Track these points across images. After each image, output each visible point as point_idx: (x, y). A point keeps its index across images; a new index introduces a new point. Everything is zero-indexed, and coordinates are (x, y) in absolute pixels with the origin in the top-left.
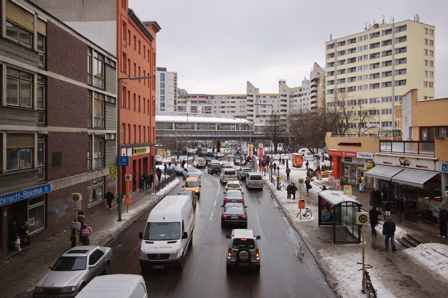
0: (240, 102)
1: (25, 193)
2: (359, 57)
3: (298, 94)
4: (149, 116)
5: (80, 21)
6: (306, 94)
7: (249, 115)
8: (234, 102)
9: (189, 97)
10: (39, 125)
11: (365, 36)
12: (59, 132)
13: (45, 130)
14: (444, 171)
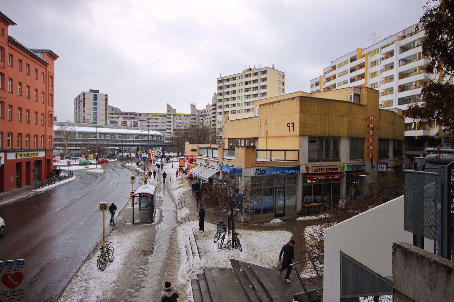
11: (242, 76)
14: (258, 174)
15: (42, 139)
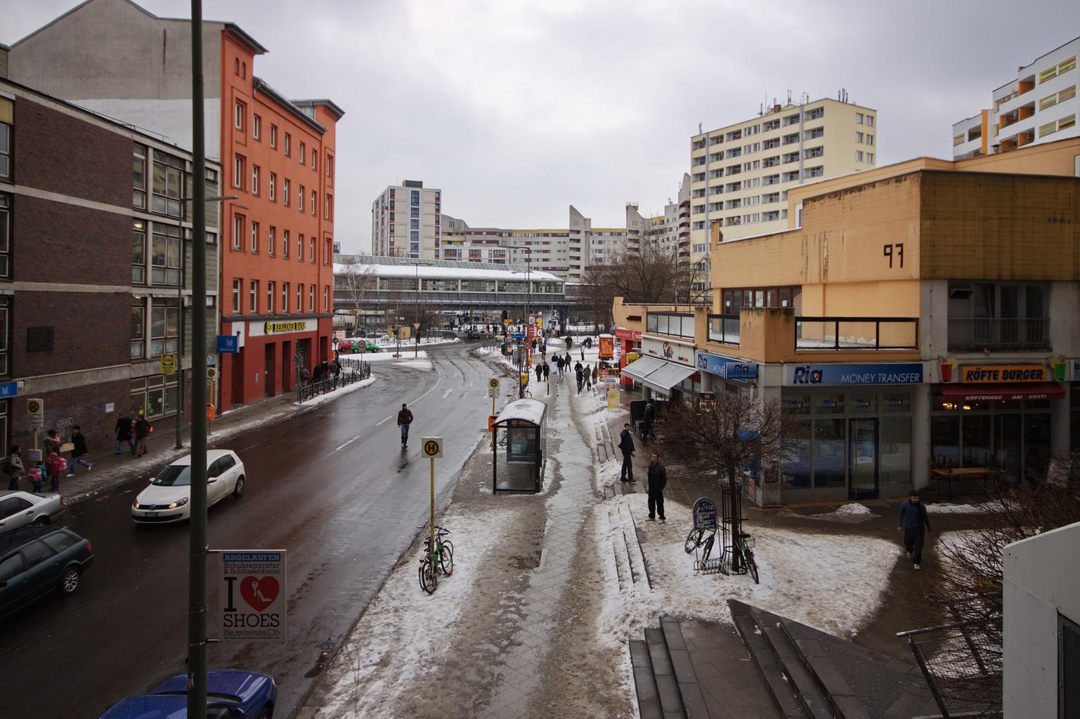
2: (745, 164)
4: (316, 266)
5: (159, 98)
7: (572, 266)
8: (547, 243)
9: (469, 233)
11: (756, 127)
14: (801, 382)
15: (284, 290)
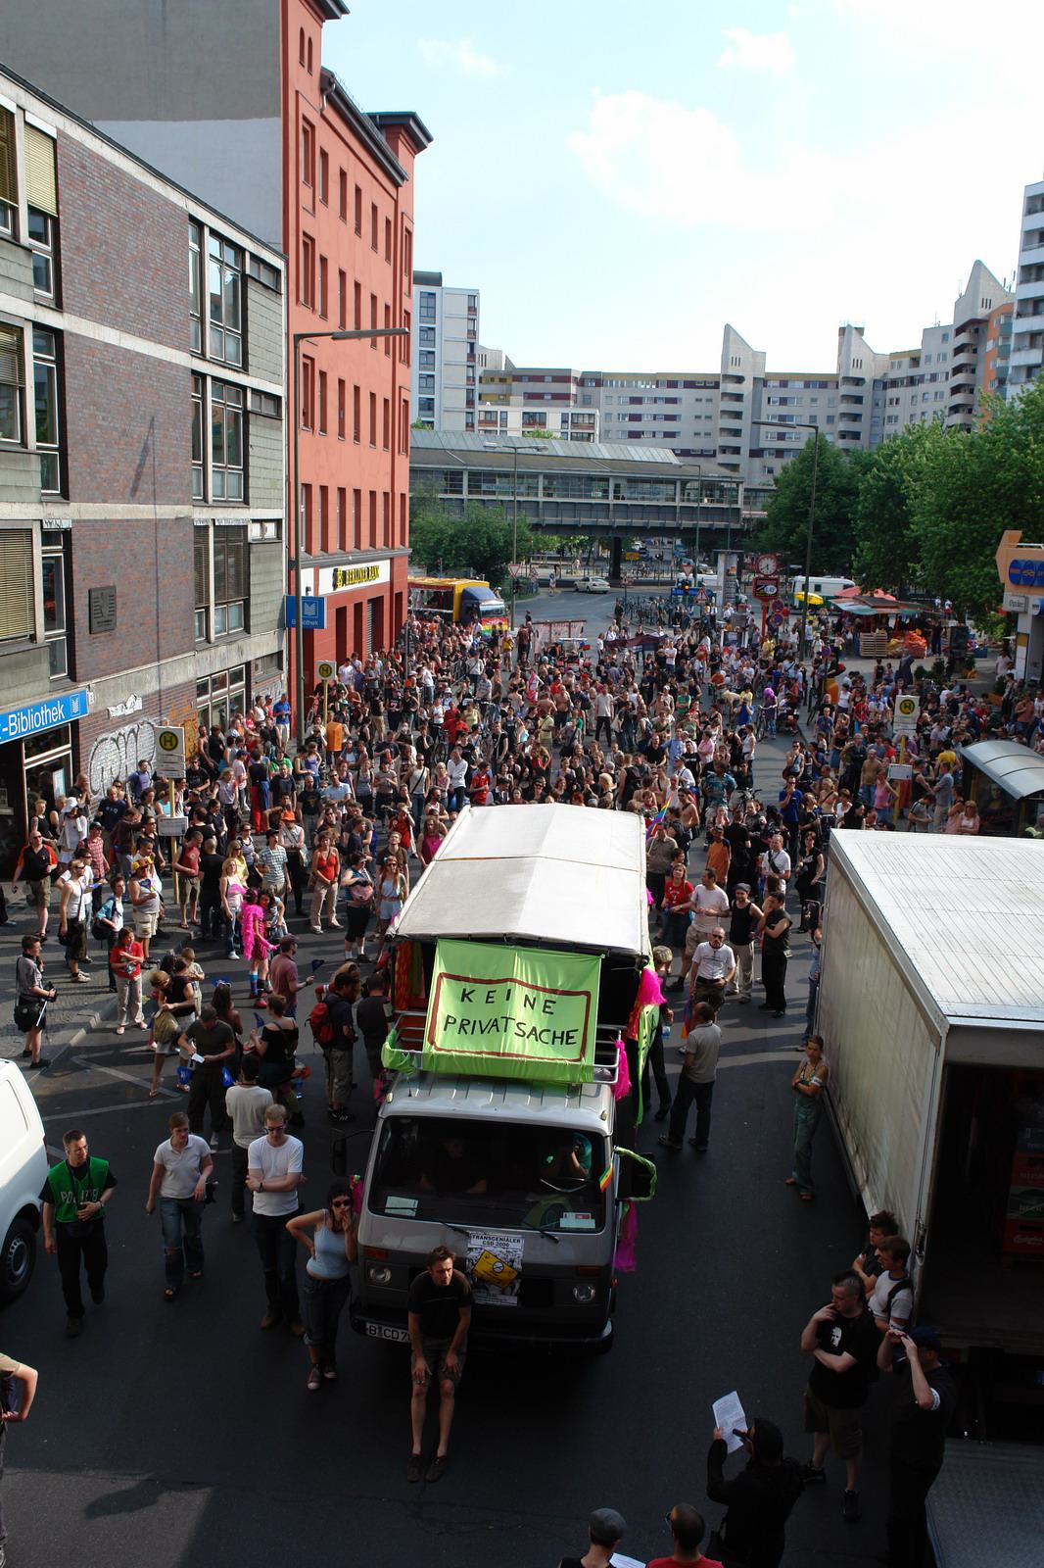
0: (697, 400)
1: (13, 720)
3: (905, 375)
6: (934, 378)
7: (724, 450)
10: (43, 498)
12: (105, 521)
13: (62, 516)
